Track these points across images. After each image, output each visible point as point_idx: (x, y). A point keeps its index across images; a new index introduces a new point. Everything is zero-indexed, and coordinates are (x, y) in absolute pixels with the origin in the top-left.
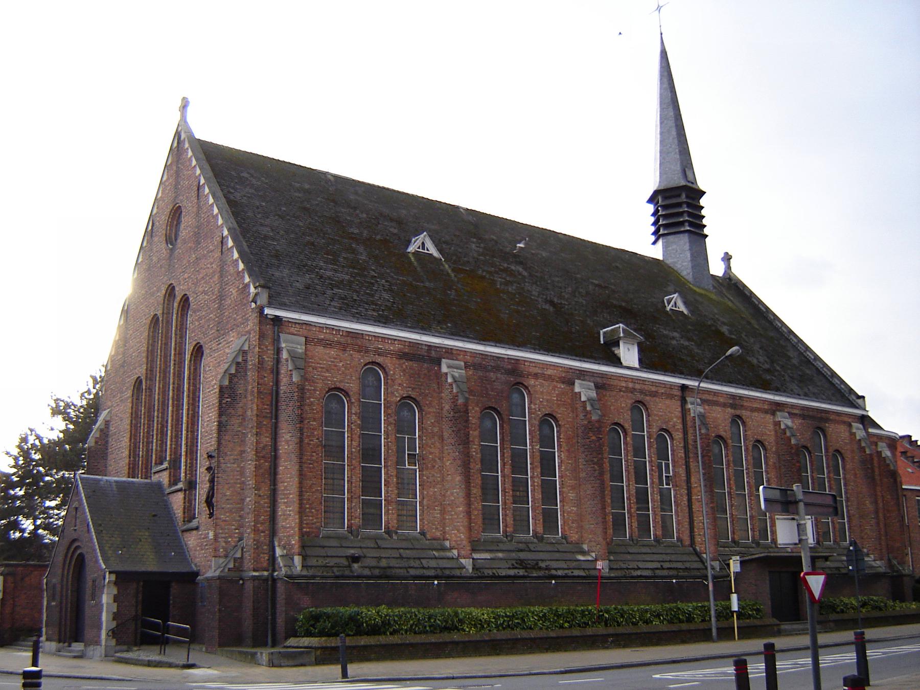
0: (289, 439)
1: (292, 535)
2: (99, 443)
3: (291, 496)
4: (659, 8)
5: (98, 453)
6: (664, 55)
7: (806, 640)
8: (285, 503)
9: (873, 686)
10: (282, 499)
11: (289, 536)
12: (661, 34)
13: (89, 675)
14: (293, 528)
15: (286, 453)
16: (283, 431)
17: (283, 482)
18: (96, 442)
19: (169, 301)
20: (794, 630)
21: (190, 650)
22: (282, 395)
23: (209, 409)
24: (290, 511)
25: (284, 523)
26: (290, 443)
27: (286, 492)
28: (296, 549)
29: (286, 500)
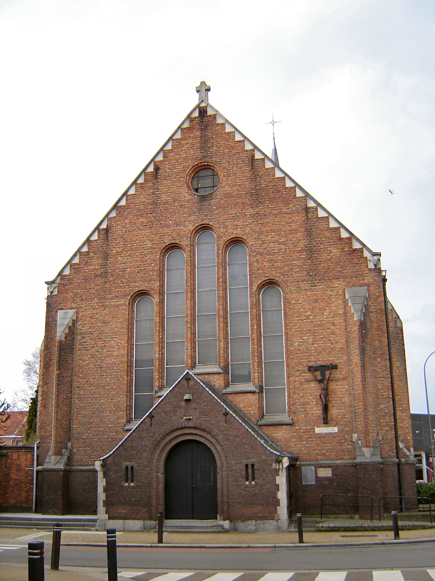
0: (399, 365)
1: (408, 433)
2: (68, 339)
3: (404, 406)
4: (273, 123)
5: (67, 347)
6: (275, 150)
7: (390, 523)
8: (400, 410)
9: (60, 570)
10: (398, 407)
11: (405, 433)
12: (274, 138)
13: (135, 548)
14: (408, 429)
15: (397, 375)
16: (394, 360)
17: (398, 396)
18: (66, 338)
19: (229, 243)
20: (74, 528)
21: (381, 518)
22: (391, 334)
23: (300, 333)
24: (404, 416)
25: (401, 425)
26: (400, 368)
27: (400, 403)
28: (411, 443)
29: (401, 409)
